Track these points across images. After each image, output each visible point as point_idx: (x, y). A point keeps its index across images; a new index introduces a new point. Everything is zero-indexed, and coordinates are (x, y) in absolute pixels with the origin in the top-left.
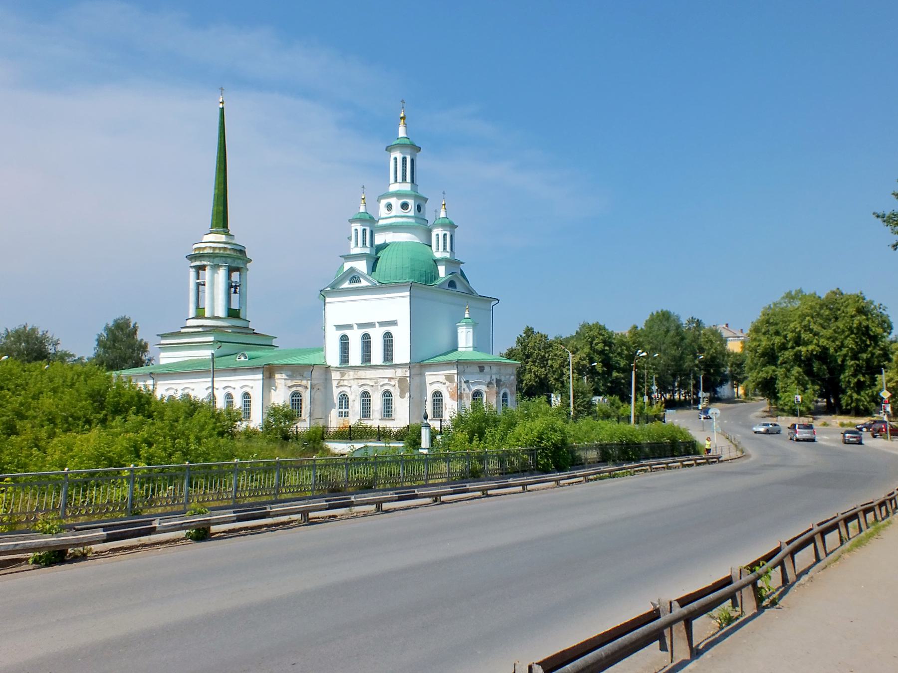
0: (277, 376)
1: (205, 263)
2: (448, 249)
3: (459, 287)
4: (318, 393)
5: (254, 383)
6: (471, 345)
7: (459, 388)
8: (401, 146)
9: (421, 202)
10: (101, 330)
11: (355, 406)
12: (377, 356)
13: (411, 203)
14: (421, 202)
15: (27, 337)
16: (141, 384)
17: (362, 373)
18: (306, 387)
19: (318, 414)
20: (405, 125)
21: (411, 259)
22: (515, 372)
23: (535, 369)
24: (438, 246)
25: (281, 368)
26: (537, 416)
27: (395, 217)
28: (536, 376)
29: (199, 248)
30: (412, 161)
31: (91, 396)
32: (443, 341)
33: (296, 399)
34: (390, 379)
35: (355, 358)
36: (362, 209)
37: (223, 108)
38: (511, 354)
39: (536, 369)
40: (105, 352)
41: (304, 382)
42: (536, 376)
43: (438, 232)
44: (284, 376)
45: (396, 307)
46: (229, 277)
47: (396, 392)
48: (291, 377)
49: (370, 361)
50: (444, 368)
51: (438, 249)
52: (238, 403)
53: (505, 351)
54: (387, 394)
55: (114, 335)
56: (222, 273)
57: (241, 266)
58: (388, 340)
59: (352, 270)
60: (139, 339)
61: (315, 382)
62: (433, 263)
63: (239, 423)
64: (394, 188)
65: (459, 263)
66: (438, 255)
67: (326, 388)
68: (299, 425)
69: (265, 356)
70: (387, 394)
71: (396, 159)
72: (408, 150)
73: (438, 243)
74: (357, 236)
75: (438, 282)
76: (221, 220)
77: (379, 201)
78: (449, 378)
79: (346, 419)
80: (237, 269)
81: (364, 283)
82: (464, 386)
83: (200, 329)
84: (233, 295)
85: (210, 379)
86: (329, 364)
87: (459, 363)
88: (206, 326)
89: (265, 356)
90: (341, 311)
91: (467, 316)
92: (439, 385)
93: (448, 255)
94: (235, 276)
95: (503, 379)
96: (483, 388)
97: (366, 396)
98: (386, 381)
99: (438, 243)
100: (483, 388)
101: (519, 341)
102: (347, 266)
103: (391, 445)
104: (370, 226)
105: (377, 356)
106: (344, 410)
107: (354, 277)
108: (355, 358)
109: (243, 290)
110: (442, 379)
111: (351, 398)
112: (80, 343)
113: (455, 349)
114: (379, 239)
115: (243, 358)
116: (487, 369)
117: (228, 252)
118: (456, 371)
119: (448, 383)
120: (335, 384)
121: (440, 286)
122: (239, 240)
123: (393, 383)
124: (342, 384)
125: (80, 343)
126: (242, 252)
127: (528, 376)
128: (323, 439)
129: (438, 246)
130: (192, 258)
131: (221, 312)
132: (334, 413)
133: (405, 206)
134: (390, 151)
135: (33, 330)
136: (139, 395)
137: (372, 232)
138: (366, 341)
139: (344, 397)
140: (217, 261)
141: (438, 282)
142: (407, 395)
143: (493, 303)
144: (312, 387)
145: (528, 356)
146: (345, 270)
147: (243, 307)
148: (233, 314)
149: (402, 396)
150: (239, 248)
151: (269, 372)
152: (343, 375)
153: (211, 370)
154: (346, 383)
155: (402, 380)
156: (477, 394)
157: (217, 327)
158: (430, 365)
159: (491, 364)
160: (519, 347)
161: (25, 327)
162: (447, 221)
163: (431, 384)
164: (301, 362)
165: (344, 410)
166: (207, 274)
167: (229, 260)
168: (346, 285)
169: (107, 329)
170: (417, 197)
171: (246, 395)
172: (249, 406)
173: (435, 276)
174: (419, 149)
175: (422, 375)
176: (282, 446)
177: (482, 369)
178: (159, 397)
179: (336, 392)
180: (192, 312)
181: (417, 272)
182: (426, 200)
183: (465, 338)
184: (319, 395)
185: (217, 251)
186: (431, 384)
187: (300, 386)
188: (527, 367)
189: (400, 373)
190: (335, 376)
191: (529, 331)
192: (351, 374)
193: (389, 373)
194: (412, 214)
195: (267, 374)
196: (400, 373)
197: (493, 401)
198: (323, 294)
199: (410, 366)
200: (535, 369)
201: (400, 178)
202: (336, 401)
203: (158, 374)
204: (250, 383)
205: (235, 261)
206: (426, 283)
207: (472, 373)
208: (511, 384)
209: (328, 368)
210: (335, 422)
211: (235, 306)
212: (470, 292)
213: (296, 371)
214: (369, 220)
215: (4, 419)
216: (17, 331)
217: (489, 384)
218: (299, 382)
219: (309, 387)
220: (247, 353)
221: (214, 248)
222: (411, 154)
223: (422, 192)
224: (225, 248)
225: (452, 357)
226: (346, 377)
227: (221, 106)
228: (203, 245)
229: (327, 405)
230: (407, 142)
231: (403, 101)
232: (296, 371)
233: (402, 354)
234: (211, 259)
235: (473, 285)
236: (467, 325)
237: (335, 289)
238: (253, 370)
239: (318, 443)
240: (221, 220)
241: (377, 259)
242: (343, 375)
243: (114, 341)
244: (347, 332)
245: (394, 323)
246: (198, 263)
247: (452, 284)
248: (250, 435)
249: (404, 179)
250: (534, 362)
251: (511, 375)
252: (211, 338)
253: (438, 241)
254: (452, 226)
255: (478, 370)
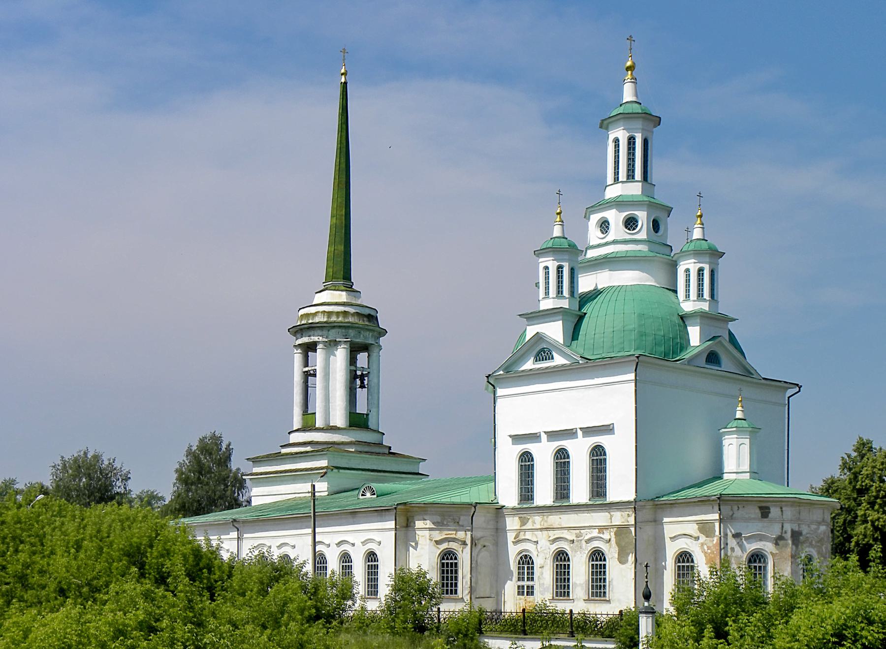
0: (419, 524)
1: (316, 339)
2: (706, 295)
3: (727, 364)
4: (484, 554)
5: (381, 535)
6: (746, 468)
7: (723, 546)
8: (627, 117)
9: (660, 215)
10: (181, 457)
11: (544, 577)
12: (580, 491)
13: (642, 216)
14: (660, 215)
15: (88, 469)
16: (201, 538)
17: (555, 519)
18: (464, 543)
19: (484, 589)
20: (634, 80)
21: (641, 316)
22: (828, 518)
23: (873, 515)
24: (688, 291)
25: (425, 510)
26: (839, 595)
27: (614, 242)
28: (876, 528)
29: (307, 315)
30: (645, 142)
31: (128, 555)
32: (697, 460)
33: (448, 564)
34: (602, 529)
35: (544, 493)
36: (557, 231)
37: (345, 83)
38: (830, 488)
39: (875, 515)
40: (188, 490)
41: (461, 535)
42: (876, 528)
43: (688, 265)
44: (429, 524)
45: (612, 401)
46: (353, 361)
47: (611, 553)
48: (439, 525)
49: (567, 497)
50: (697, 509)
51: (688, 296)
52: (333, 565)
53: (819, 484)
54: (597, 556)
55: (199, 462)
56: (341, 355)
57: (371, 341)
58: (598, 456)
59: (538, 337)
60: (234, 468)
61: (478, 534)
62: (677, 320)
63: (350, 603)
64: (612, 192)
65: (725, 319)
66: (688, 307)
67: (496, 544)
68: (443, 607)
69: (403, 489)
70: (597, 556)
71: (616, 141)
72: (639, 124)
73: (688, 285)
74: (547, 278)
75: (687, 355)
76: (341, 271)
77: (587, 217)
78: (705, 528)
79: (530, 598)
80: (365, 348)
81: (559, 360)
82: (732, 542)
83: (309, 449)
84: (359, 390)
85: (310, 531)
86: (501, 503)
87: (722, 501)
88: (317, 443)
89: (403, 489)
90: (523, 410)
91: (739, 415)
92: (688, 541)
93: (705, 306)
94: (362, 359)
95: (805, 530)
96: (768, 547)
97: (562, 559)
98: (595, 533)
99: (688, 285)
100: (768, 547)
101: (845, 466)
102: (531, 331)
103: (553, 643)
104: (569, 261)
105: (580, 491)
106: (526, 583)
107: (543, 350)
108: (544, 493)
109: (374, 381)
110: (693, 529)
111: (538, 562)
112: (153, 474)
113: (717, 475)
114: (586, 284)
115: (368, 495)
116: (774, 512)
117: (351, 319)
118: (716, 516)
119: (703, 538)
120: (511, 537)
121: (690, 361)
122: (365, 300)
123: (606, 536)
124: (522, 537)
125: (153, 474)
126: (372, 318)
127: (860, 529)
128: (481, 632)
129: (688, 291)
130: (298, 331)
131: (339, 419)
132: (510, 587)
133: (630, 223)
134: (607, 129)
135: (97, 457)
136: (197, 553)
137: (572, 271)
138: (562, 459)
139: (526, 561)
140: (333, 334)
141: (687, 355)
142: (631, 558)
143: (790, 392)
144: (474, 543)
145: (862, 491)
146: (527, 338)
147: (374, 410)
148: (357, 421)
149: (622, 560)
150: (367, 312)
151: (405, 517)
152: (524, 522)
153: (310, 514)
154: (528, 535)
155: (621, 530)
156: (756, 558)
157: (334, 443)
158: (673, 504)
159: (782, 502)
160: (847, 476)
161: (85, 454)
162: (705, 245)
163: (673, 539)
164: (456, 500)
165: (526, 583)
166: (319, 357)
167: (352, 333)
168: (529, 365)
169: (189, 453)
170: (651, 206)
171: (371, 556)
172: (376, 573)
173: (683, 343)
174: (657, 121)
175: (657, 522)
176: (413, 642)
177: (765, 512)
178: (225, 556)
179: (513, 552)
180: (297, 423)
181: (650, 339)
182: (669, 211)
183: (736, 455)
184: (484, 556)
185: (334, 319)
186: (673, 539)
187: (454, 540)
188: (860, 513)
189: (619, 518)
190: (512, 523)
191: (864, 448)
192: (537, 520)
193: (600, 518)
194: (643, 235)
195: (402, 520)
196: (619, 518)
197: (787, 571)
198: (492, 382)
199: (635, 506)
200: (873, 515)
201: (623, 176)
202: (513, 566)
203: (244, 522)
204: (376, 536)
205: (361, 333)
206: (665, 357)
207: (747, 520)
208: (821, 541)
209: (500, 510)
210: (512, 603)
211: (361, 408)
212: (748, 372)
213: (448, 515)
214: (569, 252)
215: (4, 588)
216: (76, 460)
217: (778, 541)
218: (452, 534)
219: (469, 542)
220: (374, 486)
221: (330, 314)
222: (643, 130)
223: (661, 197)
224: (345, 313)
225: (712, 490)
226: (529, 526)
227: (343, 80)
228: (313, 310)
229: (499, 578)
230: (637, 108)
231: (630, 38)
232: (448, 515)
233: (622, 484)
234: (325, 332)
235: (753, 359)
236: (739, 431)
237: (510, 373)
238: (380, 513)
239: (472, 639)
240: (341, 271)
241: (581, 318)
242: (524, 522)
243: (200, 473)
244: (531, 447)
245: (608, 429)
246: (305, 340)
247: (712, 358)
248: (365, 623)
249: (631, 176)
250: (872, 504)
251: (819, 523)
252: (324, 463)
253: (688, 281)
254: (715, 254)
255: (758, 512)
